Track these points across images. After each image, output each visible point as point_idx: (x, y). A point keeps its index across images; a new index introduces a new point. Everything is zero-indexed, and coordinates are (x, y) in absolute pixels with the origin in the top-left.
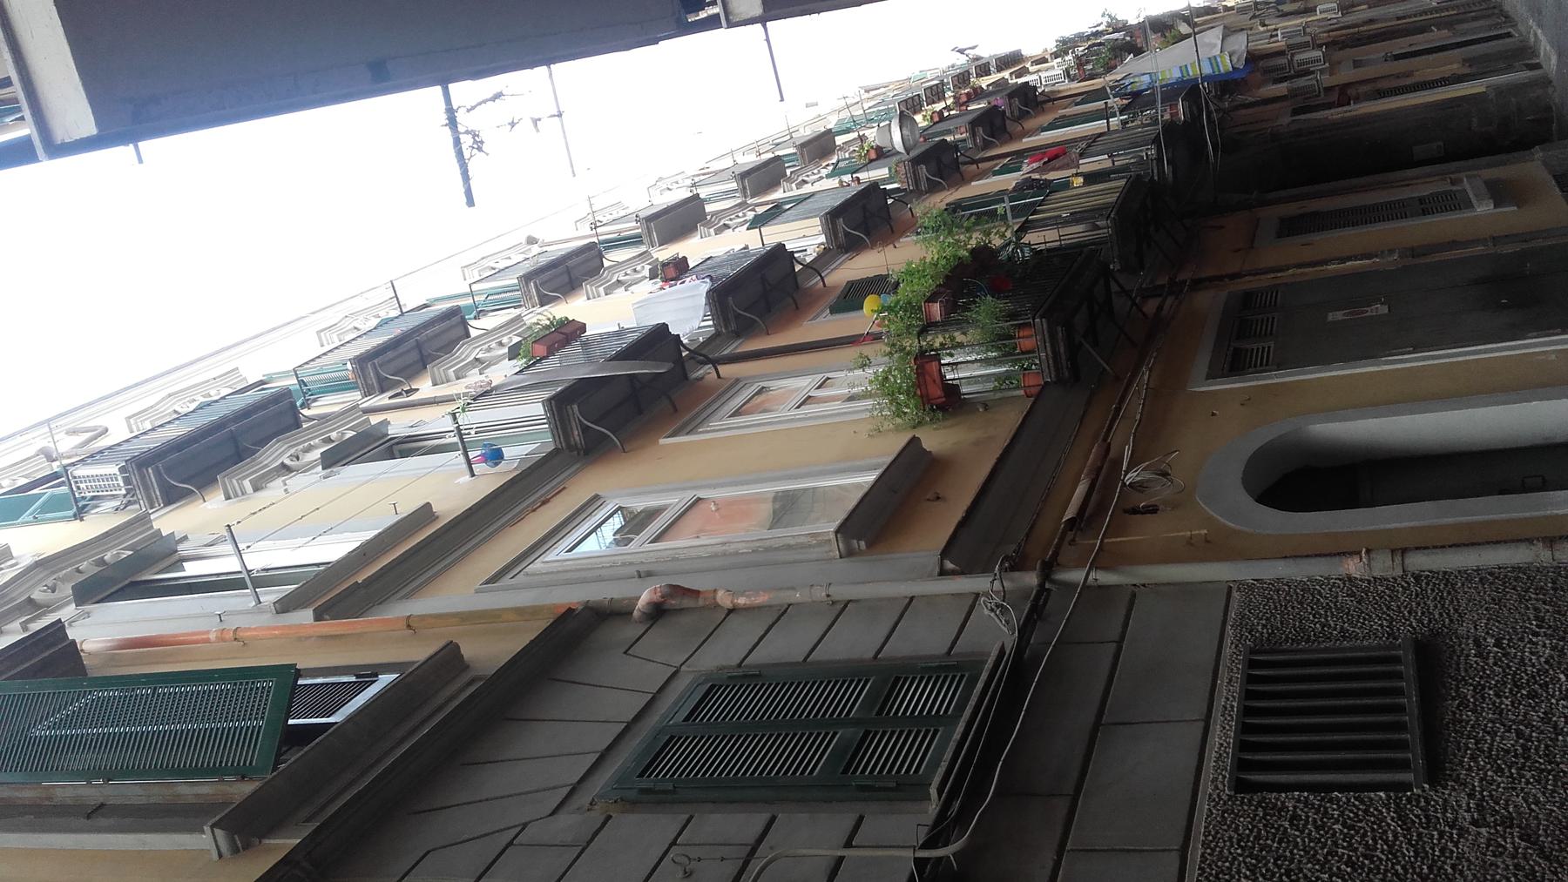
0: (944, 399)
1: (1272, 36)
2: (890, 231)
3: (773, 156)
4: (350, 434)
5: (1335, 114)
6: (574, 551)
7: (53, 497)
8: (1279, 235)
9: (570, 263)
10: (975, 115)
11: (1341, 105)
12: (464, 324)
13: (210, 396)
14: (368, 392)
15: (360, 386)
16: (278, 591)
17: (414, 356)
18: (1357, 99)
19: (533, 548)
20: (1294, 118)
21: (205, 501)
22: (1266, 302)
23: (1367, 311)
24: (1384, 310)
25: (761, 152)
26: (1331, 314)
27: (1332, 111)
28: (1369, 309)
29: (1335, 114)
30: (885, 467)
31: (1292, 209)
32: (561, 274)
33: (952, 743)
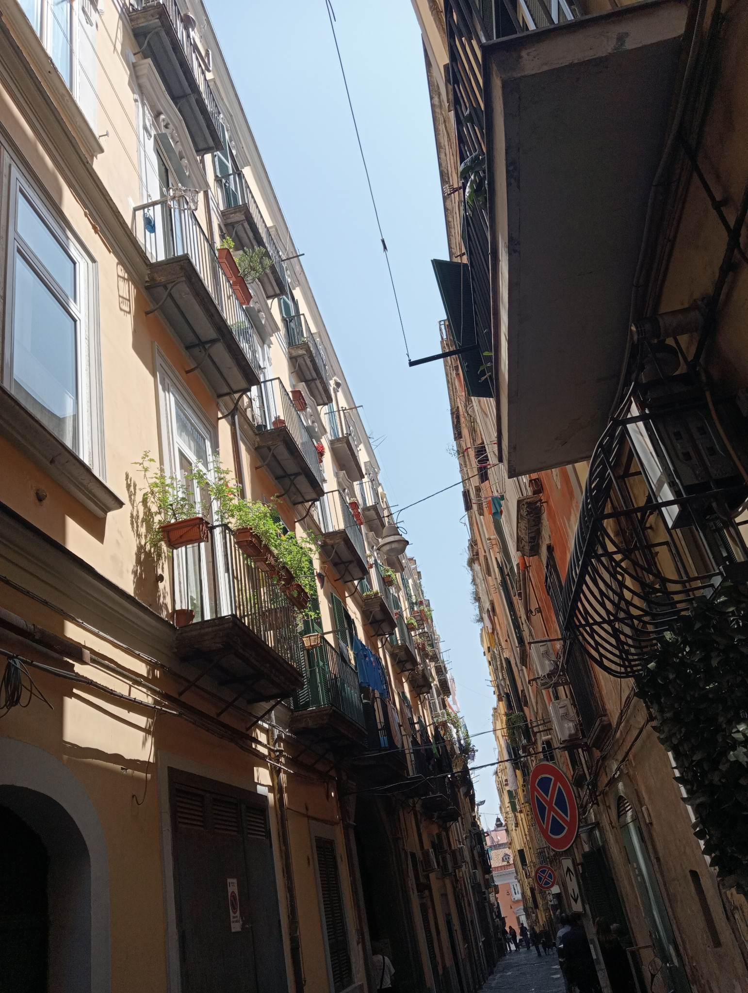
0: (272, 631)
1: (460, 842)
2: (148, 309)
3: (364, 474)
4: (263, 322)
5: (411, 883)
6: (20, 194)
7: (227, 167)
8: (319, 840)
9: (318, 382)
10: (413, 653)
11: (417, 885)
12: (324, 404)
13: (286, 271)
14: (223, 215)
15: (229, 210)
16: (37, 29)
17: (309, 377)
18: (421, 897)
19: (8, 138)
20: (409, 854)
21: (135, 54)
22: (198, 816)
23: (235, 913)
24: (236, 927)
25: (374, 482)
26: (235, 881)
27: (414, 880)
28: (238, 914)
29: (411, 883)
30: (101, 479)
31: (341, 850)
32: (312, 376)
33: (97, 631)
